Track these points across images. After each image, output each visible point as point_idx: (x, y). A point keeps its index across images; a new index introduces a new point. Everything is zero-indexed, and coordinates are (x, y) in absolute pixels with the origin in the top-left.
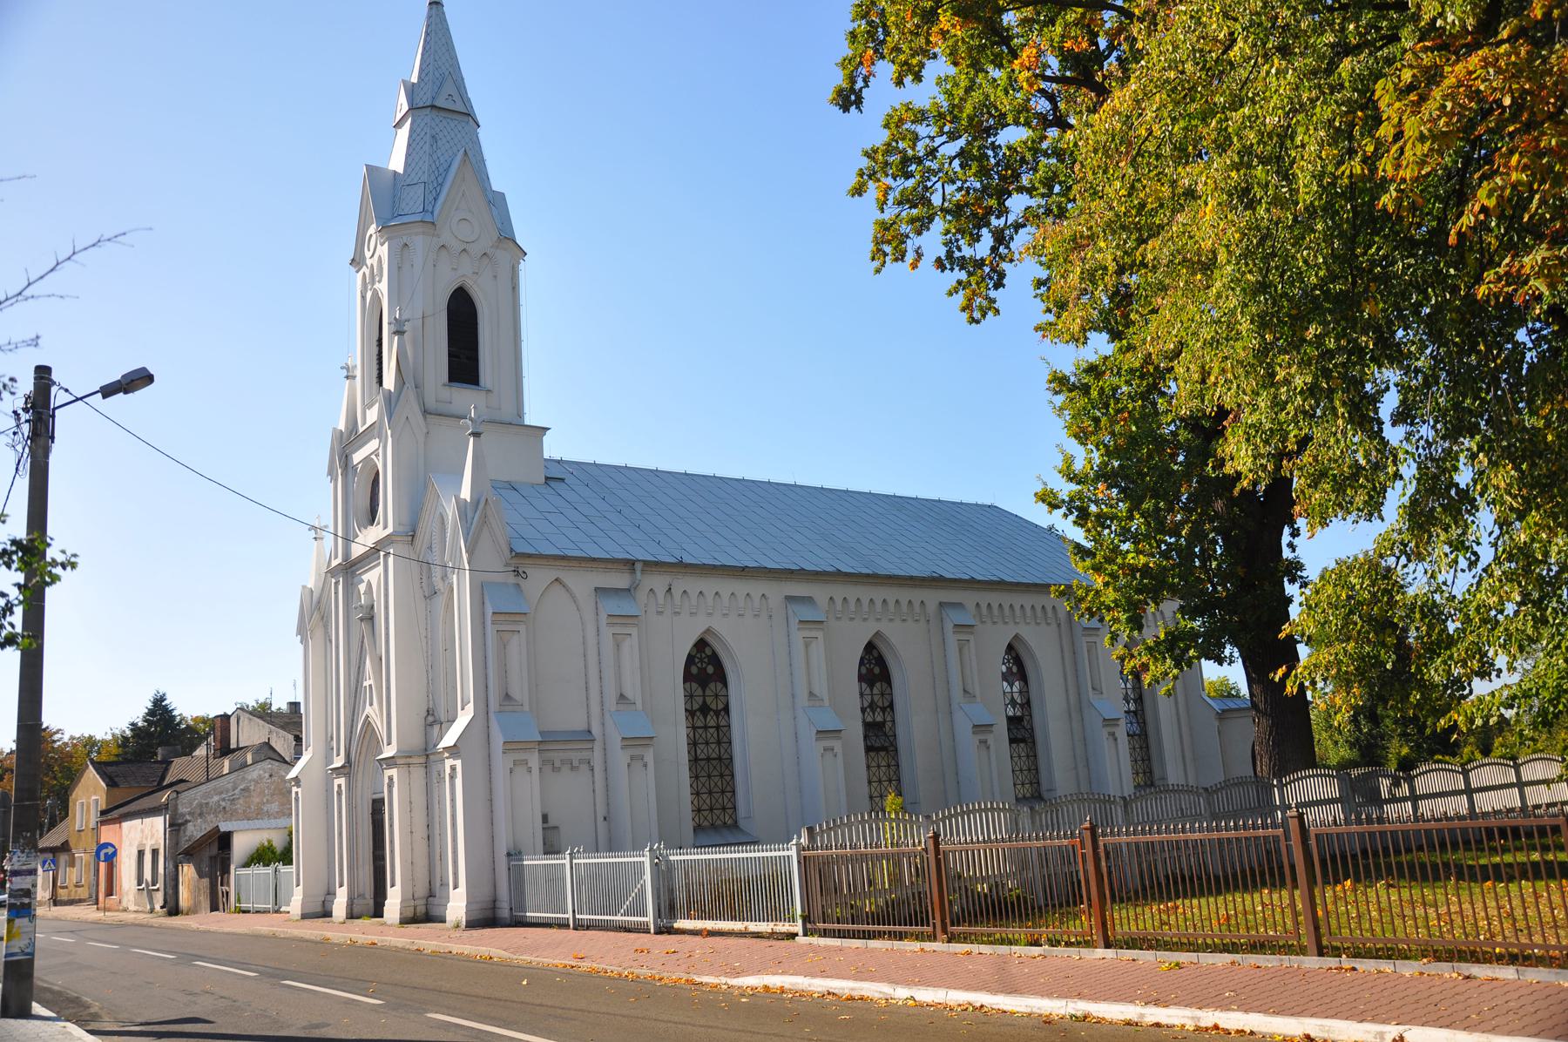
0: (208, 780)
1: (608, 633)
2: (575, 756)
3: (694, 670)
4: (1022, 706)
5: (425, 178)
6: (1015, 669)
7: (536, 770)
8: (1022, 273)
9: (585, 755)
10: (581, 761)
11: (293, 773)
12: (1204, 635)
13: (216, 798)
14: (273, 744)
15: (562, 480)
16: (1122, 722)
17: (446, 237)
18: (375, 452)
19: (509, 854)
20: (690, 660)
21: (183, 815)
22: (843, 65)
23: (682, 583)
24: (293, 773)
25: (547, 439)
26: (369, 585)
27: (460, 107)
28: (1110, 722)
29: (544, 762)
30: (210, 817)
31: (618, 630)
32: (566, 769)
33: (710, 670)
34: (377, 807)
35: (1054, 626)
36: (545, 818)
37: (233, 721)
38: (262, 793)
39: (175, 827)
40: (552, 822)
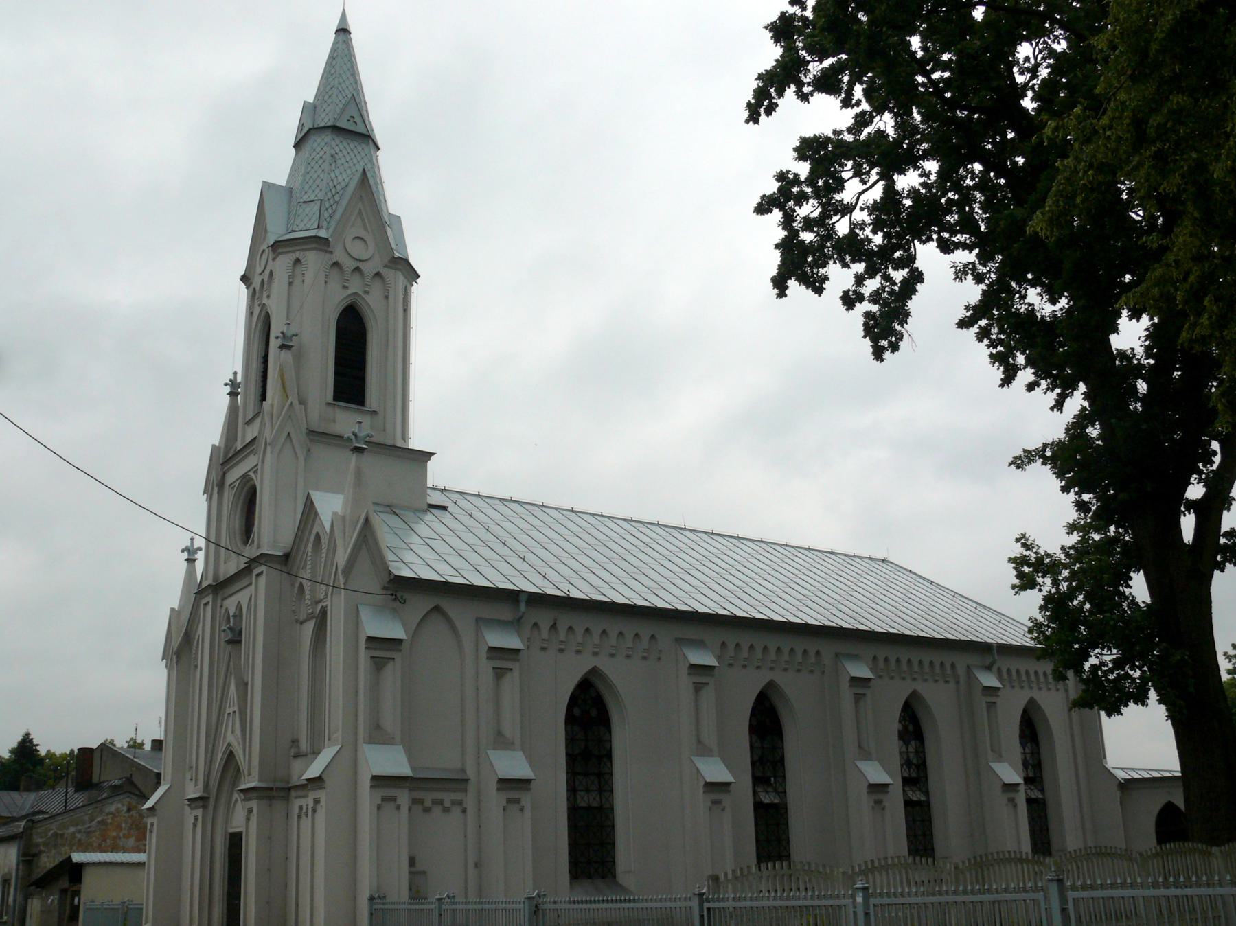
0: (66, 811)
1: (487, 675)
2: (448, 797)
3: (577, 711)
4: (918, 767)
5: (321, 196)
6: (911, 728)
7: (404, 809)
8: (1063, 557)
9: (457, 796)
10: (454, 802)
11: (149, 804)
12: (882, 230)
13: (72, 829)
14: (135, 780)
15: (444, 508)
16: (1022, 788)
17: (339, 255)
18: (255, 469)
19: (371, 899)
20: (573, 701)
21: (37, 845)
22: (760, 77)
23: (565, 620)
24: (149, 804)
25: (431, 464)
26: (239, 606)
27: (363, 131)
28: (1010, 788)
29: (416, 802)
30: (65, 849)
31: (499, 664)
32: (437, 810)
33: (594, 713)
34: (235, 842)
35: (952, 685)
36: (412, 862)
37: (97, 756)
38: (119, 827)
39: (28, 858)
40: (419, 867)
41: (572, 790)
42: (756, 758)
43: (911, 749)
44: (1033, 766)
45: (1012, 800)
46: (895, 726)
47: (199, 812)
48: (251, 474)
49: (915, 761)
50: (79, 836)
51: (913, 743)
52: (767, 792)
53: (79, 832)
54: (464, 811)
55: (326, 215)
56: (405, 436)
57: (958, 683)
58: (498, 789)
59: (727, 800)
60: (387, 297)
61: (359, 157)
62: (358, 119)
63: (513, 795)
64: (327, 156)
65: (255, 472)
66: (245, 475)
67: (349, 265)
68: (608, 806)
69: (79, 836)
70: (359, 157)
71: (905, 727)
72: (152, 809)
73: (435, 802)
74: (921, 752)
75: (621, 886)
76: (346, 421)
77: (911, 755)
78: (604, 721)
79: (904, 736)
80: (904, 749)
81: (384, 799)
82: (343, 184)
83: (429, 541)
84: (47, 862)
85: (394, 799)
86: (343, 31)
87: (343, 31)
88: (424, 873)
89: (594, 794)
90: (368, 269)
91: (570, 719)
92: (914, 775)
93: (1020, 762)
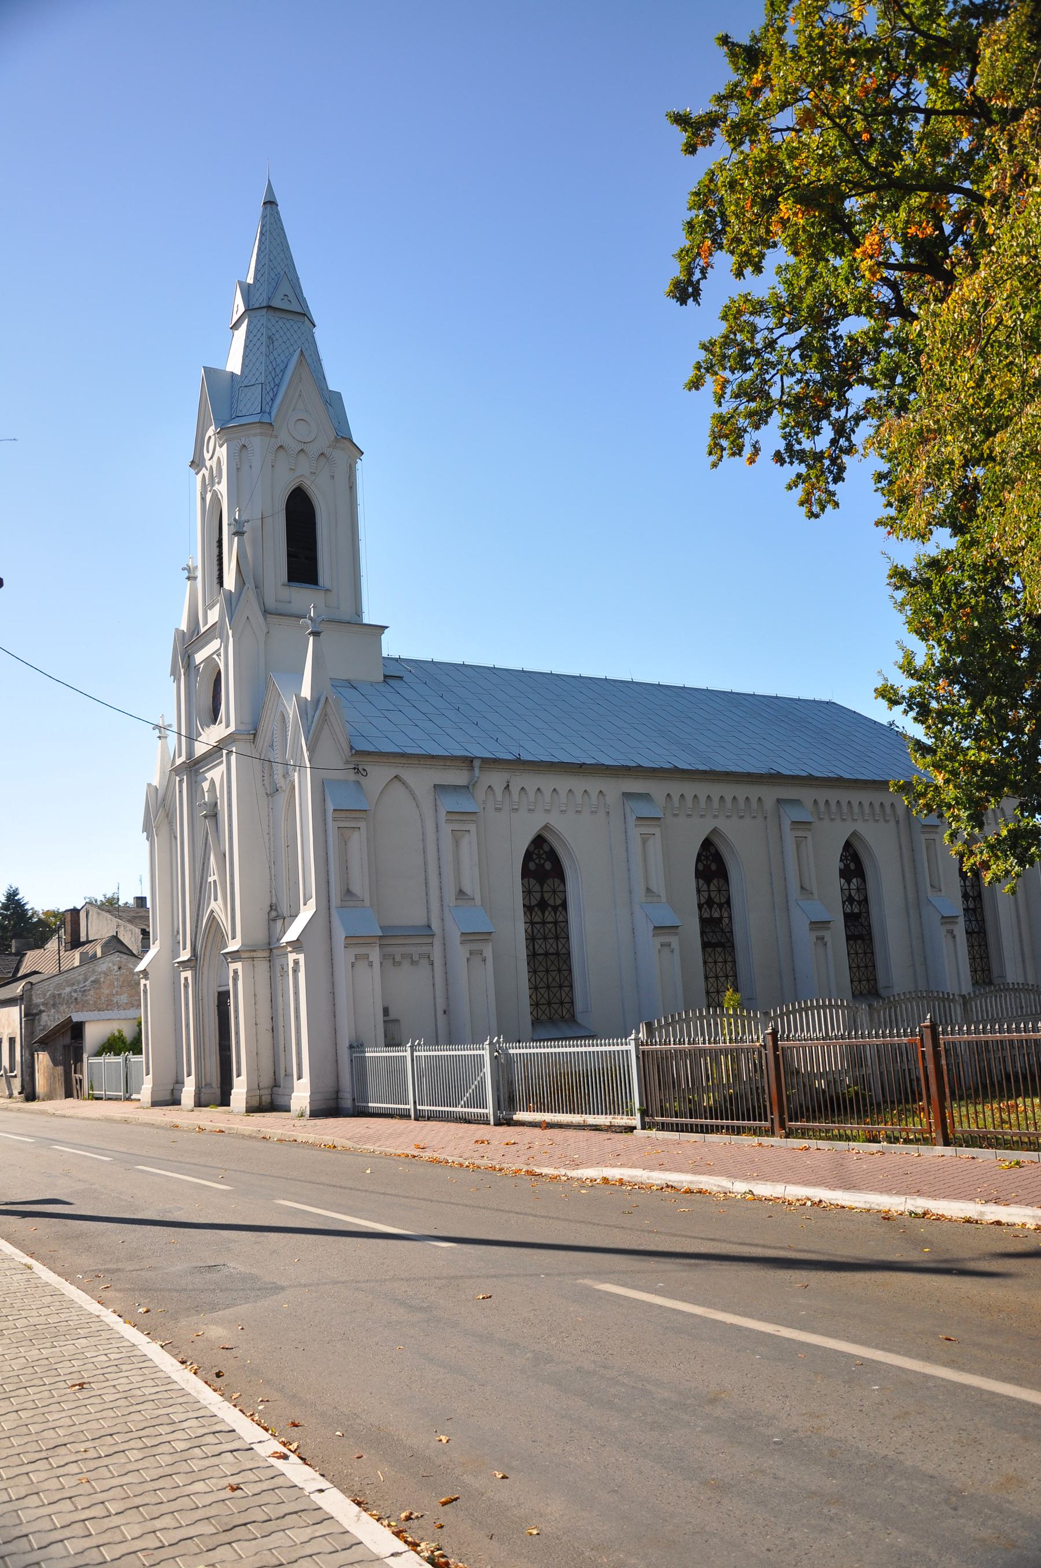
3: (532, 866)
4: (859, 903)
5: (262, 379)
6: (852, 866)
9: (425, 949)
11: (141, 966)
13: (68, 990)
15: (400, 678)
16: (961, 920)
17: (284, 438)
18: (217, 652)
20: (528, 856)
21: (37, 1005)
23: (520, 780)
24: (141, 966)
29: (384, 957)
32: (406, 965)
35: (892, 823)
38: (112, 985)
39: (30, 1017)
40: (393, 1015)
41: (703, 933)
42: (703, 901)
43: (852, 886)
44: (974, 898)
45: (951, 932)
46: (836, 865)
47: (188, 974)
48: (215, 656)
49: (856, 898)
50: (75, 995)
51: (854, 880)
52: (714, 932)
53: (75, 991)
54: (484, 960)
55: (268, 399)
56: (359, 613)
57: (898, 822)
58: (811, 930)
59: (827, 935)
60: (333, 477)
61: (296, 337)
62: (292, 297)
63: (475, 946)
64: (264, 339)
65: (219, 655)
66: (210, 657)
67: (295, 447)
68: (851, 942)
69: (75, 995)
70: (296, 337)
71: (847, 866)
72: (145, 973)
73: (403, 956)
74: (863, 889)
75: (579, 1024)
76: (304, 598)
77: (853, 893)
78: (559, 873)
79: (845, 874)
80: (846, 886)
81: (471, 953)
82: (282, 366)
83: (443, 711)
84: (50, 1020)
85: (367, 956)
86: (270, 203)
87: (270, 203)
88: (397, 1020)
89: (551, 941)
90: (313, 450)
91: (526, 873)
92: (856, 911)
93: (960, 895)
